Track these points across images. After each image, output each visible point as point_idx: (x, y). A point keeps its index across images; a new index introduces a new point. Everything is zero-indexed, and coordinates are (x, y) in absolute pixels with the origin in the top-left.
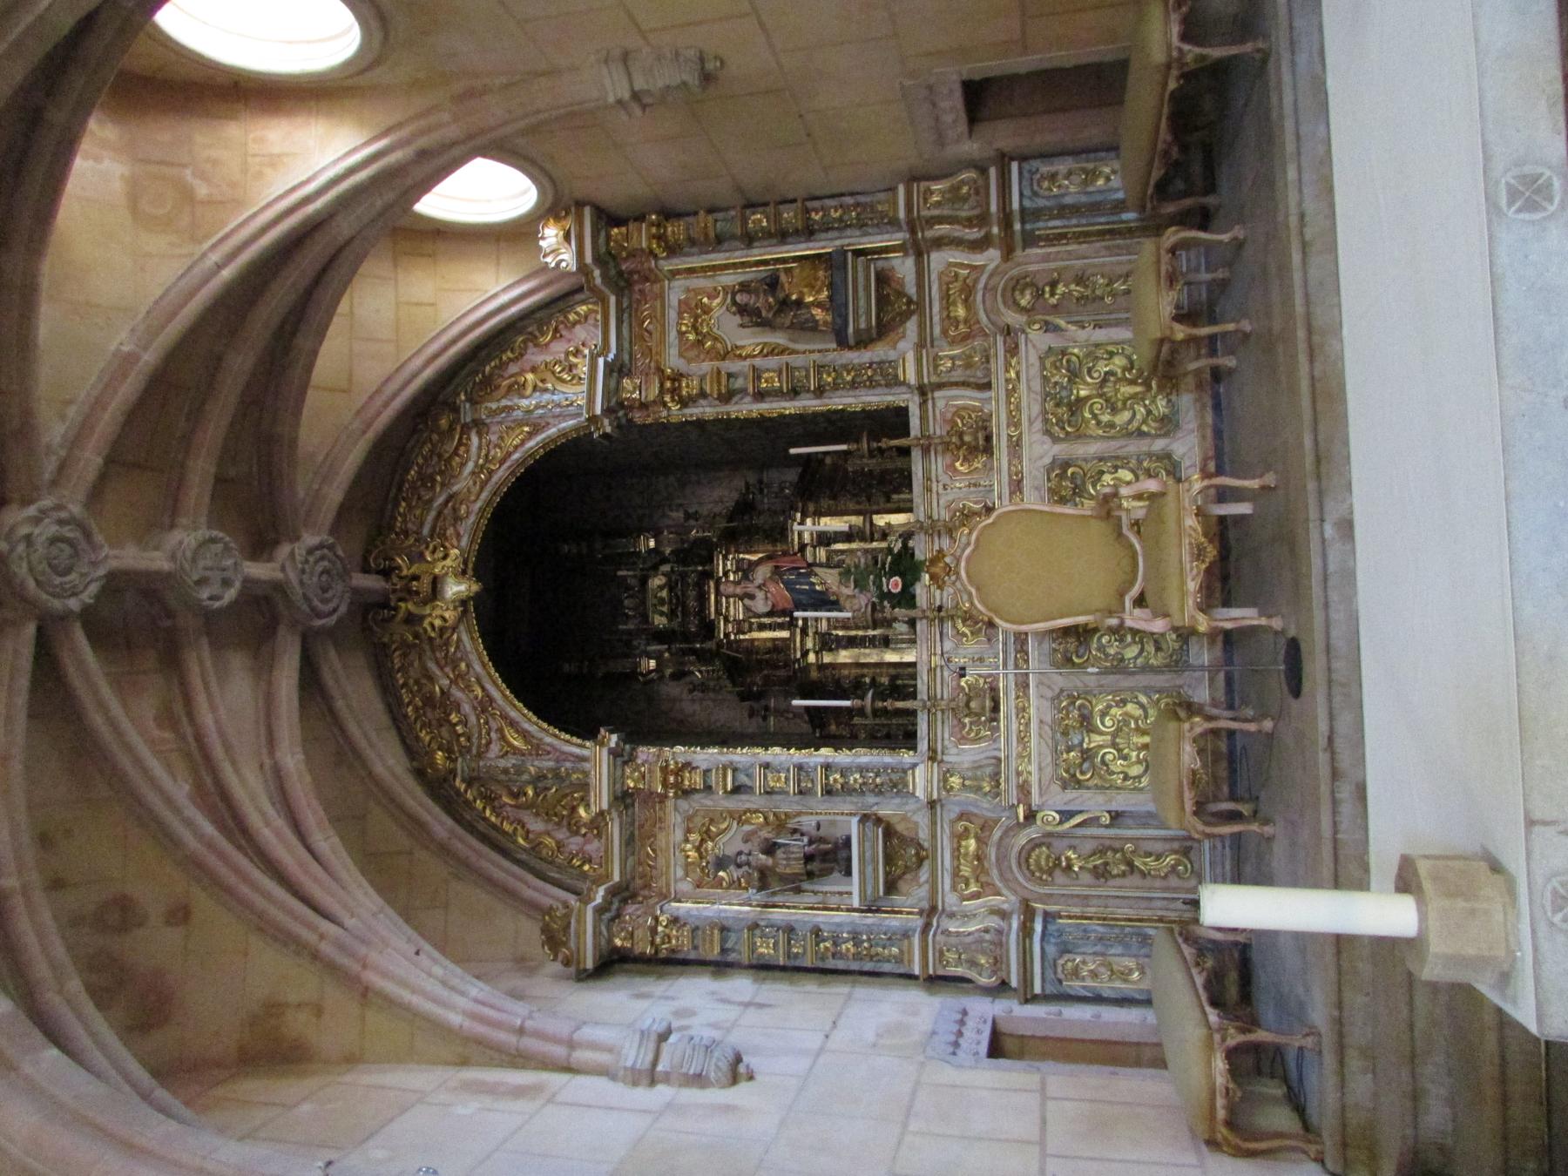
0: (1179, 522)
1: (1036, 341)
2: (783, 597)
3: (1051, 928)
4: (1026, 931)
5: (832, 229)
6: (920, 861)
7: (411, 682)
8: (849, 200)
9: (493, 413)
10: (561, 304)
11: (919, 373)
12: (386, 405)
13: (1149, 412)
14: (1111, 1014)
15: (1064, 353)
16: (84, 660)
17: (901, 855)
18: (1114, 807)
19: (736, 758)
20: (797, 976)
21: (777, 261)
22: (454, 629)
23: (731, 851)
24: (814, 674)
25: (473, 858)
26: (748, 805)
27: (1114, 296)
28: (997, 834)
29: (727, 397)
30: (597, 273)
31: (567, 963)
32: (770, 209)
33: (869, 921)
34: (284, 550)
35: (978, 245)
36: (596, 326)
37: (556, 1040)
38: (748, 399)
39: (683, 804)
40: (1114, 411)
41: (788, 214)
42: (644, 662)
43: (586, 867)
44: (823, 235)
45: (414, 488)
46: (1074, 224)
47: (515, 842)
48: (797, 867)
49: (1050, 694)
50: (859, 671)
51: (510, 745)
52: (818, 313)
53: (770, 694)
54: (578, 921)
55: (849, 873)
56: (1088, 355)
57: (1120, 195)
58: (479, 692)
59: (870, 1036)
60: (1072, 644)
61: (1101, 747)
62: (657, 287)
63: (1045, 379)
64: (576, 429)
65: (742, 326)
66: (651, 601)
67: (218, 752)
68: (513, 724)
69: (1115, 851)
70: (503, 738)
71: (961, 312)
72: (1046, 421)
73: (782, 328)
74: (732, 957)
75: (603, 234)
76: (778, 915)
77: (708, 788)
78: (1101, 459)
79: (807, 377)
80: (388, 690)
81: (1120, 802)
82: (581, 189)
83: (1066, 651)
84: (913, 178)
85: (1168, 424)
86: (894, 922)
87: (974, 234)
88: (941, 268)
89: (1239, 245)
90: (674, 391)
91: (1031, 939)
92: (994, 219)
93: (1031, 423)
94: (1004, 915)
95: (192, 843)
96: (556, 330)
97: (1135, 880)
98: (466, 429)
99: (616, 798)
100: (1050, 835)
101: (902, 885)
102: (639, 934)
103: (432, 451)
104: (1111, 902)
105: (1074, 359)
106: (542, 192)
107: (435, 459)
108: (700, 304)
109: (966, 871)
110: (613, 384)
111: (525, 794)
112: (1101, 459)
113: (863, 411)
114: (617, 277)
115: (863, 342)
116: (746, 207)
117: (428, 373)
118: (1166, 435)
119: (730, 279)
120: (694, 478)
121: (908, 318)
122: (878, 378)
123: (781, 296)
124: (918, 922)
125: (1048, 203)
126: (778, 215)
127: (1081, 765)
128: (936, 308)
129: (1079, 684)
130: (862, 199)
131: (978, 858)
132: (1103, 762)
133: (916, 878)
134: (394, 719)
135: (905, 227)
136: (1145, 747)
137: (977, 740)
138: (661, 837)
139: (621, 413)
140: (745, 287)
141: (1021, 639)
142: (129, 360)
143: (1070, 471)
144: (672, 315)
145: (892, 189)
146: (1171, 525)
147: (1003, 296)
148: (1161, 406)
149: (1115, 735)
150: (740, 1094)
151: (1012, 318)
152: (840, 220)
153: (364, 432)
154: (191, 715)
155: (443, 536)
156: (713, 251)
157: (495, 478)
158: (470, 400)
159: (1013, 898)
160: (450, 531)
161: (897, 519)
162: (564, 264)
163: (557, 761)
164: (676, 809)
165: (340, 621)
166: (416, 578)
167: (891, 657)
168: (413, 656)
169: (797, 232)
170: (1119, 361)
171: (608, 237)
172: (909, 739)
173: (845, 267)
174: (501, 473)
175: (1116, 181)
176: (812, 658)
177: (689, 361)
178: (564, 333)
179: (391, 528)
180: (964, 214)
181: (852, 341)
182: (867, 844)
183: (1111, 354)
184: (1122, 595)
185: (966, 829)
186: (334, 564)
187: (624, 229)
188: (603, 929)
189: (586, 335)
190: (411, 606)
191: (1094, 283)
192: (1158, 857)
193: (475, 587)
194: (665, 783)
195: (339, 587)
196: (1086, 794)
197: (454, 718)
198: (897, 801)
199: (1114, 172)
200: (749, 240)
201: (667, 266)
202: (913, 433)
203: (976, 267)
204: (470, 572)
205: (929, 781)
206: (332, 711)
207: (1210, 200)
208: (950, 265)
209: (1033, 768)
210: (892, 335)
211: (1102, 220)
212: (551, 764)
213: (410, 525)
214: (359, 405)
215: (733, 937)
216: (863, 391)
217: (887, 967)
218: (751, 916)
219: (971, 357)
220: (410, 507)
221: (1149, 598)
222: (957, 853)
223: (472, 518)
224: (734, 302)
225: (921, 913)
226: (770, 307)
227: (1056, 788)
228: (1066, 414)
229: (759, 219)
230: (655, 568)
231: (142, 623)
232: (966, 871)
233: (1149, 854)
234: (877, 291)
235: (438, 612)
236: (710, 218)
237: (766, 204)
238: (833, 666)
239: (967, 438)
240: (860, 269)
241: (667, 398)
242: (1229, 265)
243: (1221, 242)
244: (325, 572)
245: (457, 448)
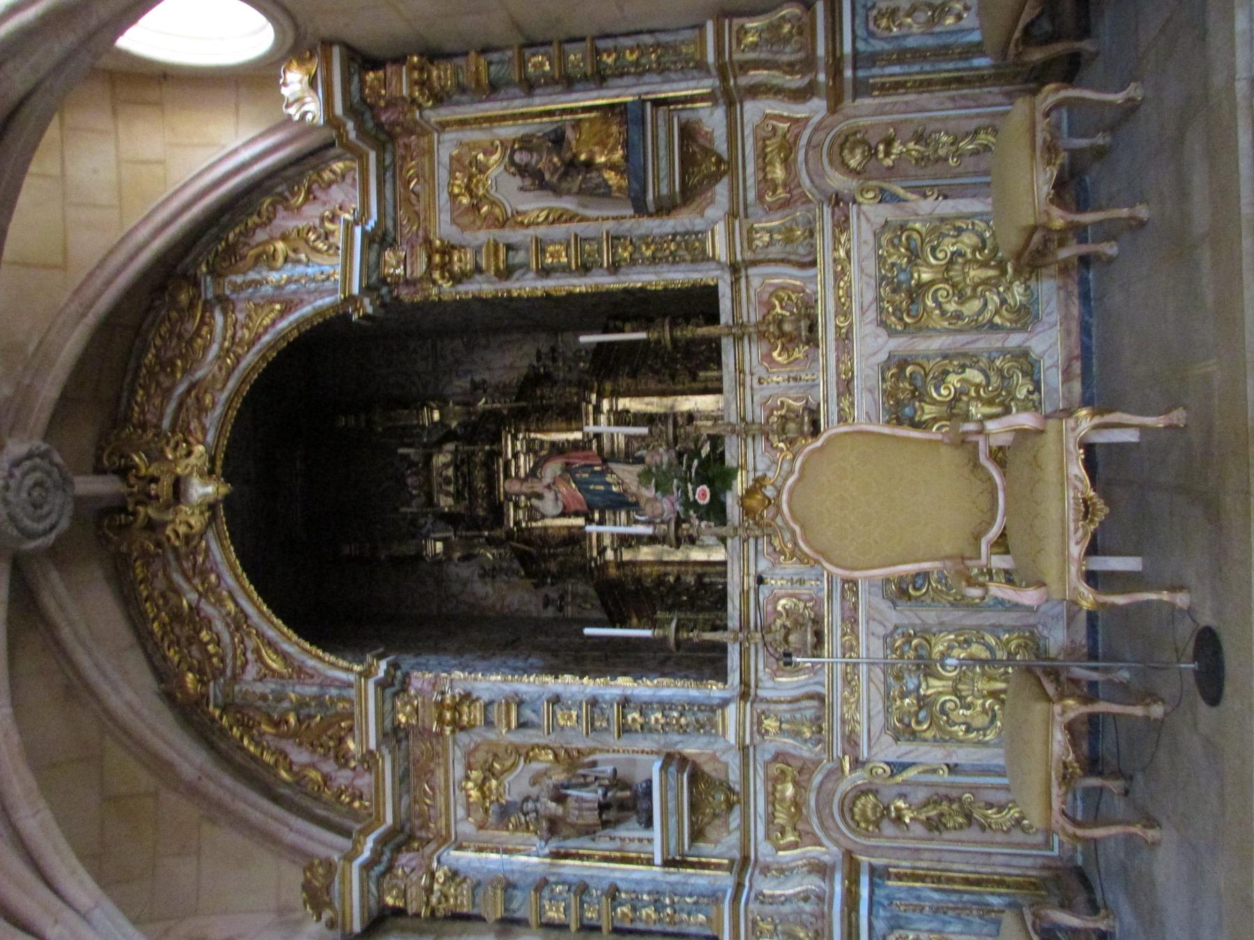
0: (1061, 468)
1: (870, 214)
2: (574, 497)
3: (880, 893)
5: (628, 74)
6: (730, 806)
7: (156, 594)
8: (647, 39)
9: (237, 288)
10: (313, 161)
12: (108, 283)
13: (1004, 302)
15: (903, 228)
18: (953, 760)
21: (564, 111)
22: (202, 535)
24: (613, 571)
25: (227, 798)
26: (536, 740)
27: (960, 156)
28: (817, 779)
29: (507, 273)
30: (350, 125)
32: (553, 50)
33: (673, 878)
35: (801, 95)
36: (353, 186)
38: (531, 275)
39: (463, 737)
40: (962, 299)
41: (575, 56)
42: (430, 544)
43: (357, 804)
44: (618, 82)
45: (151, 373)
46: (914, 70)
47: (277, 775)
48: (592, 817)
49: (881, 631)
50: (662, 569)
51: (267, 667)
52: (611, 177)
54: (342, 882)
55: (649, 824)
56: (931, 231)
57: (976, 37)
58: (231, 606)
61: (940, 693)
62: (424, 141)
63: (881, 260)
64: (333, 306)
65: (522, 189)
66: (436, 479)
68: (270, 644)
69: (951, 801)
70: (260, 659)
71: (779, 173)
72: (881, 310)
73: (568, 192)
75: (356, 79)
78: (945, 357)
79: (600, 251)
80: (129, 600)
81: (962, 756)
82: (325, 26)
85: (1025, 316)
87: (795, 81)
88: (757, 119)
89: (1131, 108)
90: (443, 267)
91: (858, 912)
92: (821, 64)
93: (863, 312)
96: (309, 191)
97: (973, 833)
98: (208, 307)
99: (385, 735)
101: (711, 832)
102: (413, 892)
103: (171, 332)
104: (947, 856)
105: (915, 236)
106: (279, 31)
107: (175, 342)
108: (474, 162)
109: (781, 818)
110: (373, 257)
111: (287, 722)
112: (945, 357)
113: (665, 289)
115: (665, 208)
116: (523, 46)
117: (158, 244)
118: (1023, 329)
119: (509, 131)
120: (483, 341)
121: (717, 181)
122: (681, 253)
123: (568, 155)
125: (887, 47)
126: (563, 56)
127: (916, 714)
128: (750, 169)
129: (917, 621)
130: (664, 38)
131: (796, 803)
132: (943, 711)
133: (727, 824)
135: (714, 72)
136: (994, 694)
138: (440, 773)
139: (384, 290)
140: (526, 143)
143: (909, 370)
144: (442, 174)
145: (701, 27)
146: (1051, 467)
147: (829, 154)
148: (1018, 293)
149: (957, 680)
151: (837, 181)
152: (637, 63)
153: (84, 315)
155: (187, 431)
156: (488, 100)
157: (243, 364)
158: (212, 271)
159: (834, 849)
160: (194, 424)
161: (704, 403)
162: (309, 117)
163: (321, 686)
164: (455, 742)
165: (59, 539)
166: (155, 480)
167: (697, 555)
168: (157, 565)
169: (585, 78)
170: (968, 240)
171: (362, 82)
172: (709, 662)
173: (643, 123)
174: (250, 359)
175: (969, 20)
176: (610, 555)
177: (463, 228)
178: (318, 194)
179: (127, 419)
180: (785, 58)
181: (651, 208)
182: (671, 794)
183: (960, 231)
184: (977, 538)
185: (783, 772)
186: (49, 474)
187: (381, 73)
188: (373, 888)
189: (345, 197)
190: (151, 512)
191: (937, 142)
192: (1001, 808)
193: (224, 489)
194: (441, 720)
195: (57, 499)
196: (924, 748)
197: (205, 636)
198: (704, 739)
199: (967, 8)
200: (530, 86)
201: (435, 116)
202: (723, 320)
203: (797, 120)
204: (219, 470)
205: (741, 724)
206: (58, 642)
207: (1086, 45)
208: (767, 117)
209: (862, 717)
210: (698, 200)
211: (951, 66)
212: (314, 690)
213: (149, 417)
214: (78, 282)
216: (666, 267)
218: (540, 869)
219: (791, 230)
220: (148, 396)
221: (1012, 541)
222: (772, 799)
223: (219, 410)
224: (512, 162)
225: (729, 868)
226: (556, 169)
227: (887, 739)
228: (904, 301)
229: (540, 62)
230: (440, 444)
232: (781, 818)
233: (990, 805)
234: (681, 147)
235: (181, 517)
236: (482, 61)
237: (550, 43)
238: (633, 563)
239: (787, 327)
240: (661, 122)
241: (437, 275)
242: (1112, 129)
243: (1111, 104)
244: (38, 484)
245: (199, 328)
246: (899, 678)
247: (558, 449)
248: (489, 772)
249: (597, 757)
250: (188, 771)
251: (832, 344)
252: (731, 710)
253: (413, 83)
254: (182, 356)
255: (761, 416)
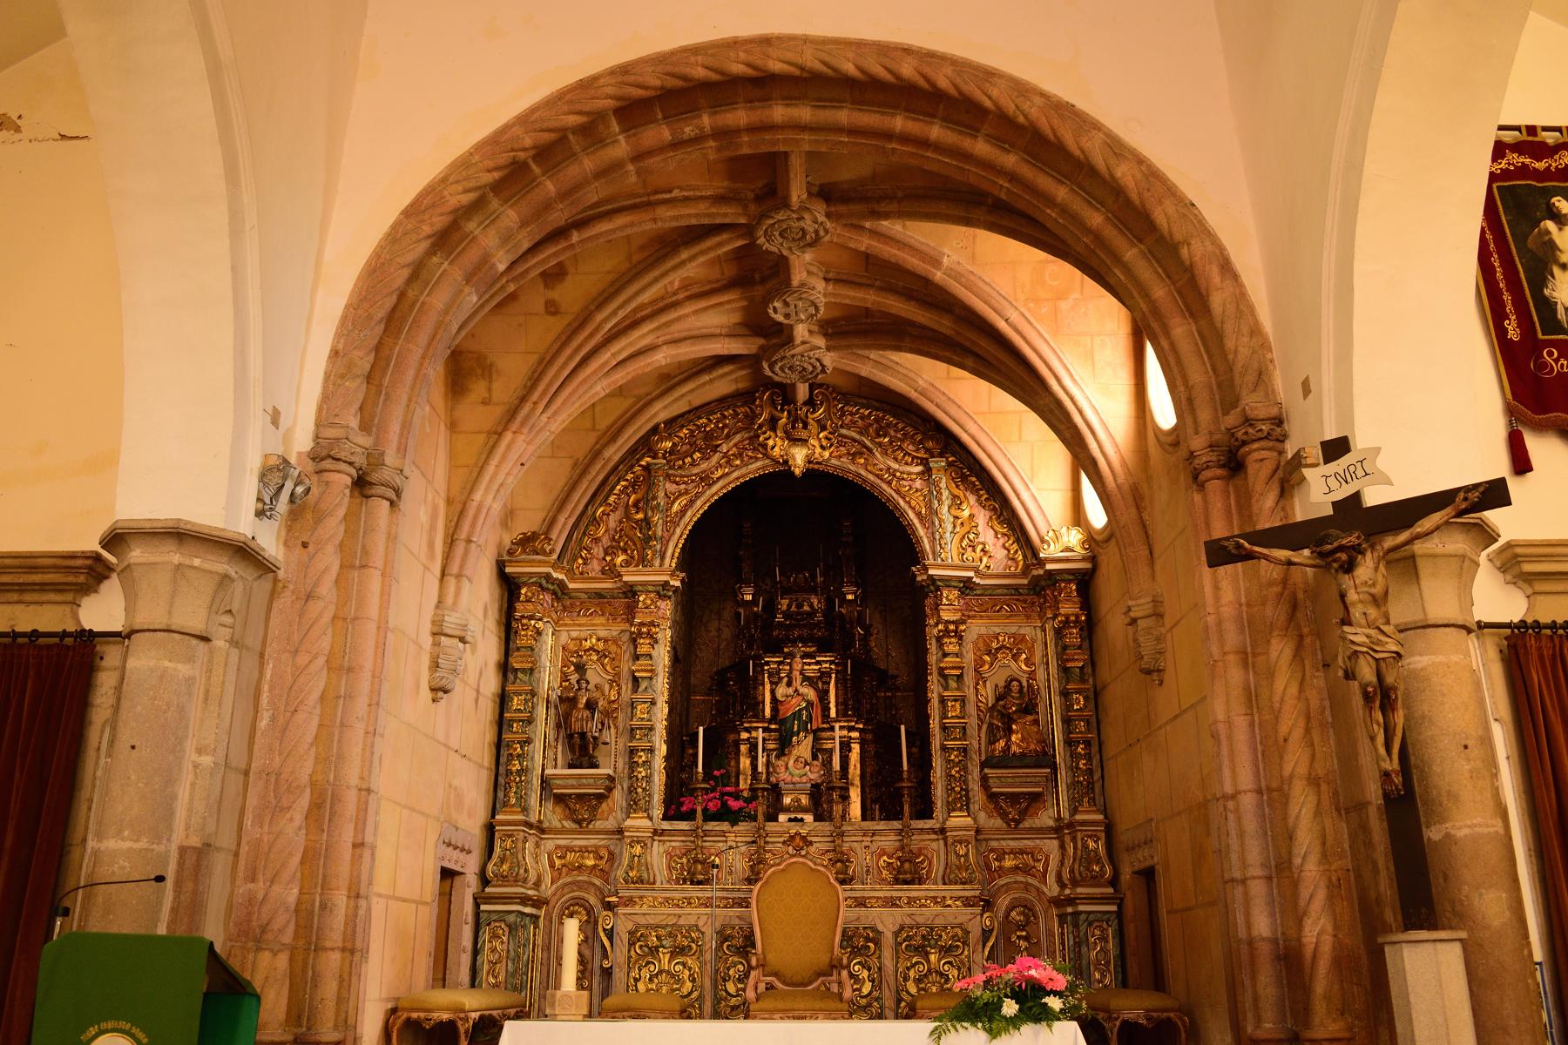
4: (525, 900)
6: (579, 822)
11: (955, 829)
14: (466, 959)
16: (729, 244)
17: (580, 807)
18: (616, 970)
19: (660, 679)
20: (496, 728)
22: (766, 456)
23: (590, 675)
25: (589, 477)
31: (510, 553)
34: (820, 342)
37: (462, 566)
39: (626, 637)
40: (918, 981)
48: (576, 727)
49: (700, 924)
53: (715, 702)
56: (962, 962)
59: (456, 783)
60: (740, 942)
66: (801, 597)
67: (664, 318)
68: (691, 502)
70: (681, 495)
71: (1008, 863)
74: (511, 677)
76: (541, 711)
77: (636, 657)
79: (955, 739)
81: (619, 976)
82: (1103, 560)
83: (733, 937)
84: (1109, 829)
86: (534, 800)
90: (947, 632)
94: (537, 885)
95: (599, 317)
98: (924, 462)
100: (596, 922)
102: (530, 606)
109: (570, 857)
114: (1037, 585)
117: (965, 438)
124: (533, 819)
132: (648, 963)
133: (567, 818)
134: (697, 408)
137: (670, 868)
138: (602, 620)
141: (744, 903)
142: (936, 262)
149: (668, 972)
150: (426, 694)
151: (1003, 902)
154: (690, 298)
155: (840, 444)
157: (884, 486)
161: (855, 808)
166: (805, 426)
171: (1069, 582)
172: (674, 811)
176: (744, 735)
184: (775, 974)
194: (642, 624)
196: (625, 950)
197: (698, 455)
205: (638, 829)
215: (526, 678)
217: (501, 794)
220: (862, 418)
222: (584, 850)
225: (540, 821)
227: (630, 926)
229: (1079, 702)
231: (757, 275)
235: (779, 442)
241: (941, 627)
246: (670, 934)
247: (823, 695)
248: (602, 655)
249: (613, 730)
250: (608, 453)
251: (888, 894)
252: (647, 823)
253: (1067, 618)
254: (891, 442)
255: (845, 847)
